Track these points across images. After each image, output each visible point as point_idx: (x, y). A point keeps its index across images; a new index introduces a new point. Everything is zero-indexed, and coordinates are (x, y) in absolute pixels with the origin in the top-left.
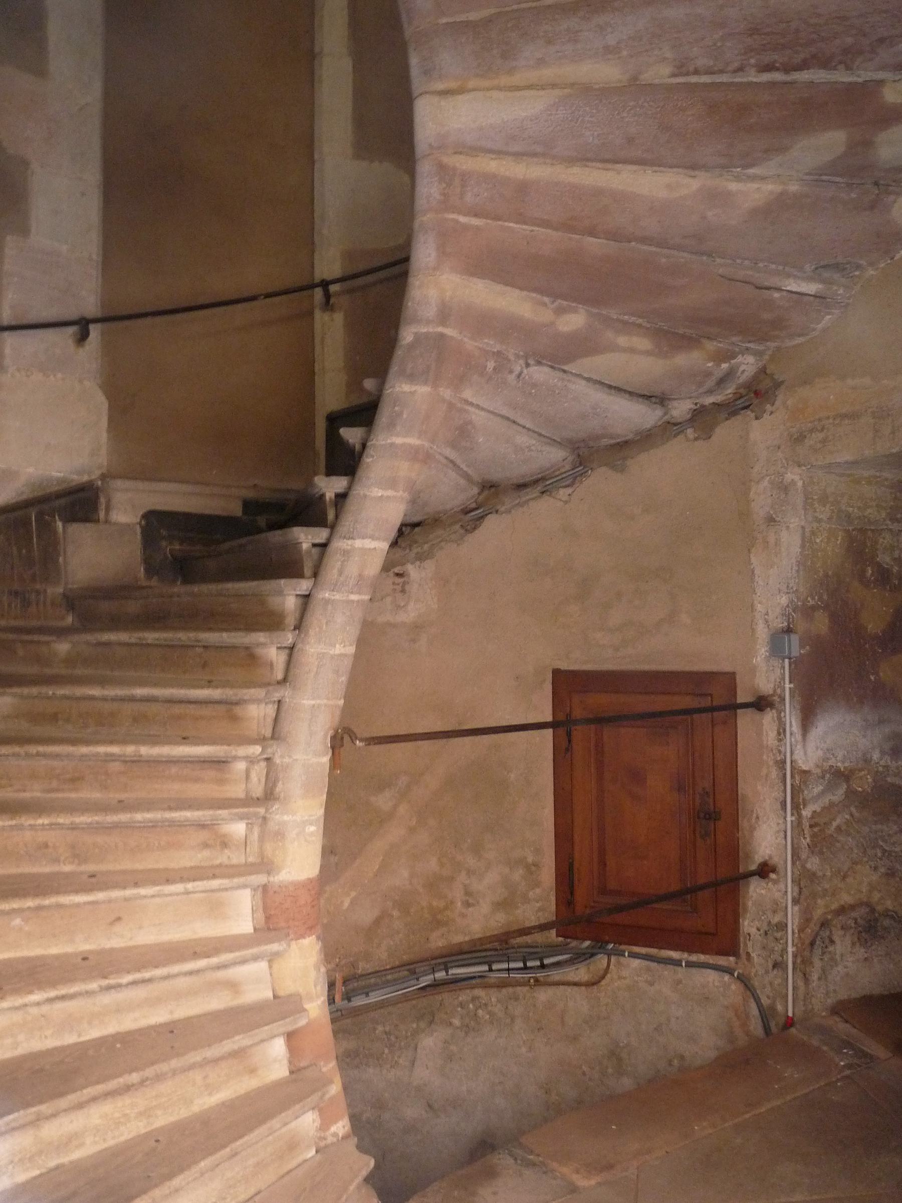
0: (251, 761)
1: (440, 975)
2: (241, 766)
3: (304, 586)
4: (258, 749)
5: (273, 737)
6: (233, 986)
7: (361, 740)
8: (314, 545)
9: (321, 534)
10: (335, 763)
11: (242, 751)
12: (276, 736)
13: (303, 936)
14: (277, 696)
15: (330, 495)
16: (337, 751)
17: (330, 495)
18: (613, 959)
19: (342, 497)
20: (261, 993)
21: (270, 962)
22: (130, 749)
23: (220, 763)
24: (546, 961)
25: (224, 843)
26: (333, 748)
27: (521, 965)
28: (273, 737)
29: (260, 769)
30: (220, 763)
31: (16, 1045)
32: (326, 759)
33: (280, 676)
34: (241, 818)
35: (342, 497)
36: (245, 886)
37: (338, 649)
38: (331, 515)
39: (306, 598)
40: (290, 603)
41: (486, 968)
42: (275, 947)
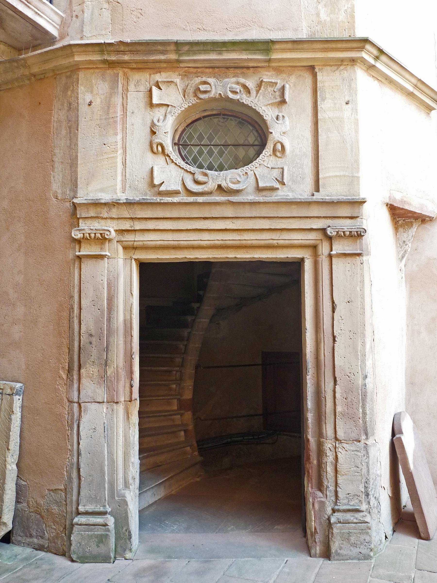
0: (177, 371)
1: (229, 440)
2: (174, 372)
3: (189, 330)
4: (178, 368)
5: (182, 366)
6: (173, 420)
7: (202, 367)
8: (192, 320)
9: (193, 318)
10: (196, 372)
11: (175, 369)
12: (184, 353)
13: (188, 411)
14: (182, 356)
15: (195, 307)
16: (97, 48)
17: (195, 307)
18: (279, 436)
19: (198, 308)
20: (179, 422)
21: (181, 416)
22: (150, 368)
23: (169, 372)
24: (259, 437)
25: (171, 389)
26: (196, 369)
27: (252, 437)
28: (182, 366)
29: (178, 374)
30: (169, 372)
31: (319, 102)
32: (194, 371)
33: (183, 351)
34: (174, 384)
35: (198, 308)
36: (175, 399)
37: (197, 345)
38: (196, 312)
39: (190, 333)
40: (186, 334)
41: (242, 438)
42: (182, 412)
